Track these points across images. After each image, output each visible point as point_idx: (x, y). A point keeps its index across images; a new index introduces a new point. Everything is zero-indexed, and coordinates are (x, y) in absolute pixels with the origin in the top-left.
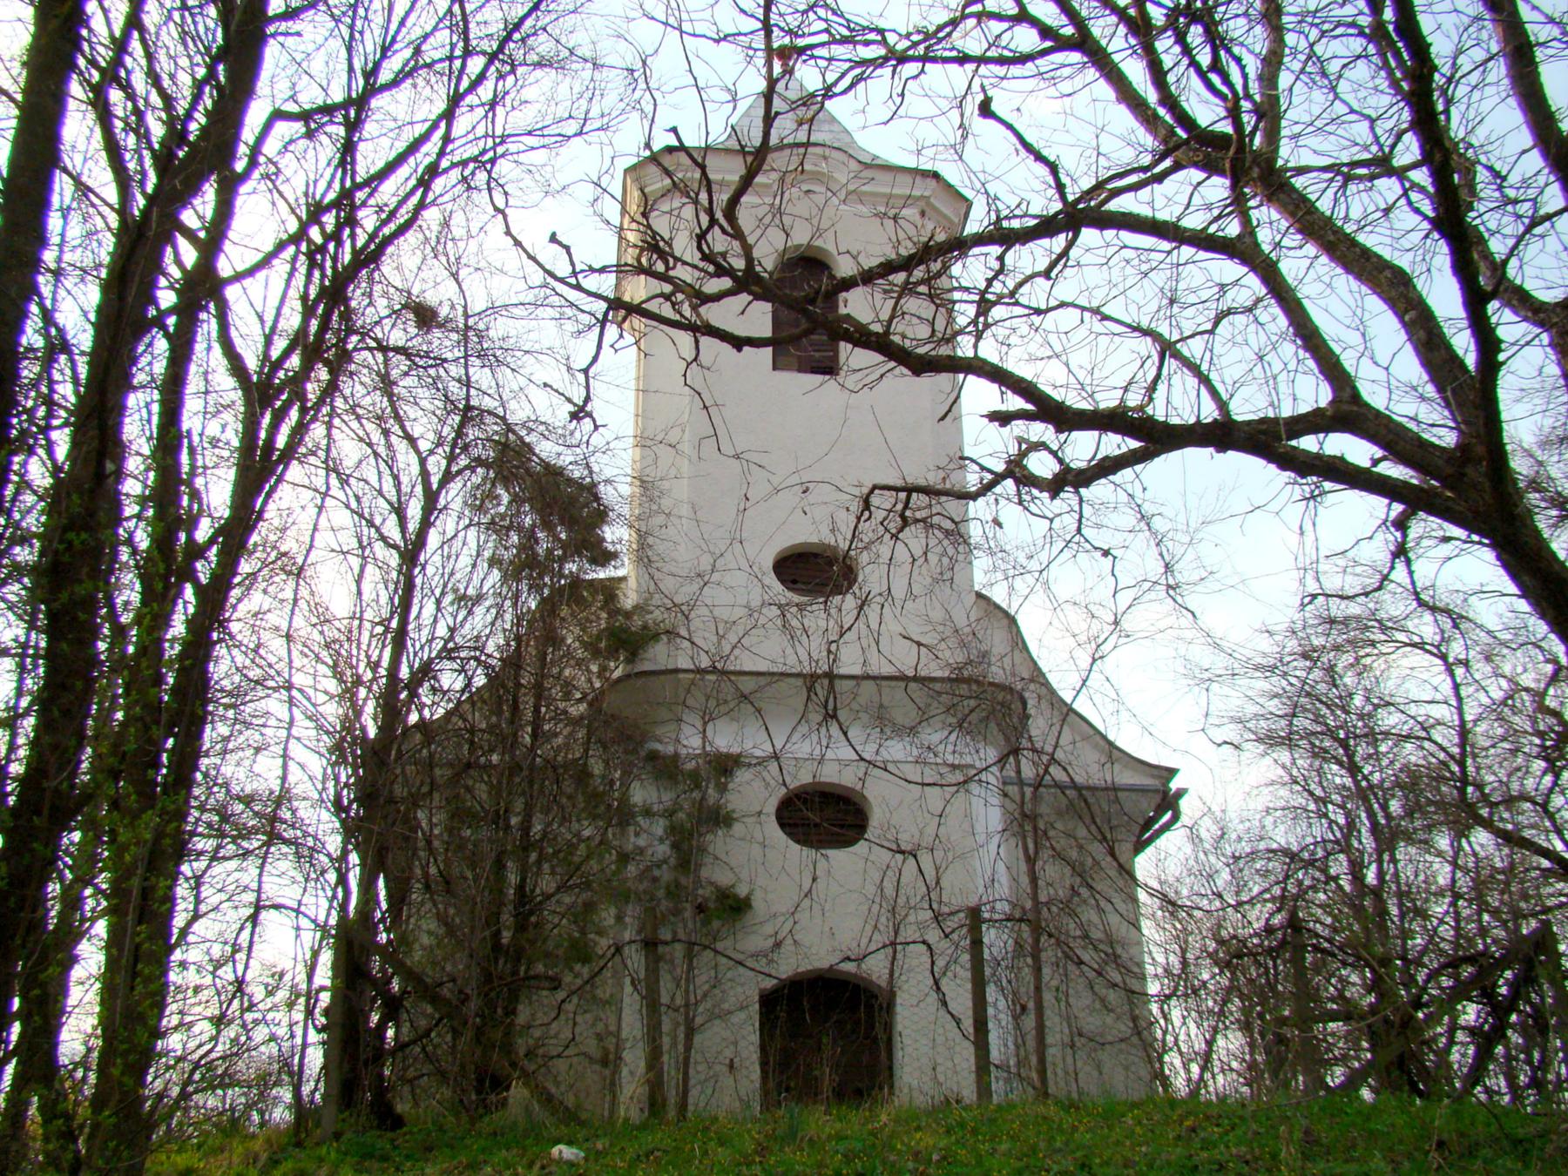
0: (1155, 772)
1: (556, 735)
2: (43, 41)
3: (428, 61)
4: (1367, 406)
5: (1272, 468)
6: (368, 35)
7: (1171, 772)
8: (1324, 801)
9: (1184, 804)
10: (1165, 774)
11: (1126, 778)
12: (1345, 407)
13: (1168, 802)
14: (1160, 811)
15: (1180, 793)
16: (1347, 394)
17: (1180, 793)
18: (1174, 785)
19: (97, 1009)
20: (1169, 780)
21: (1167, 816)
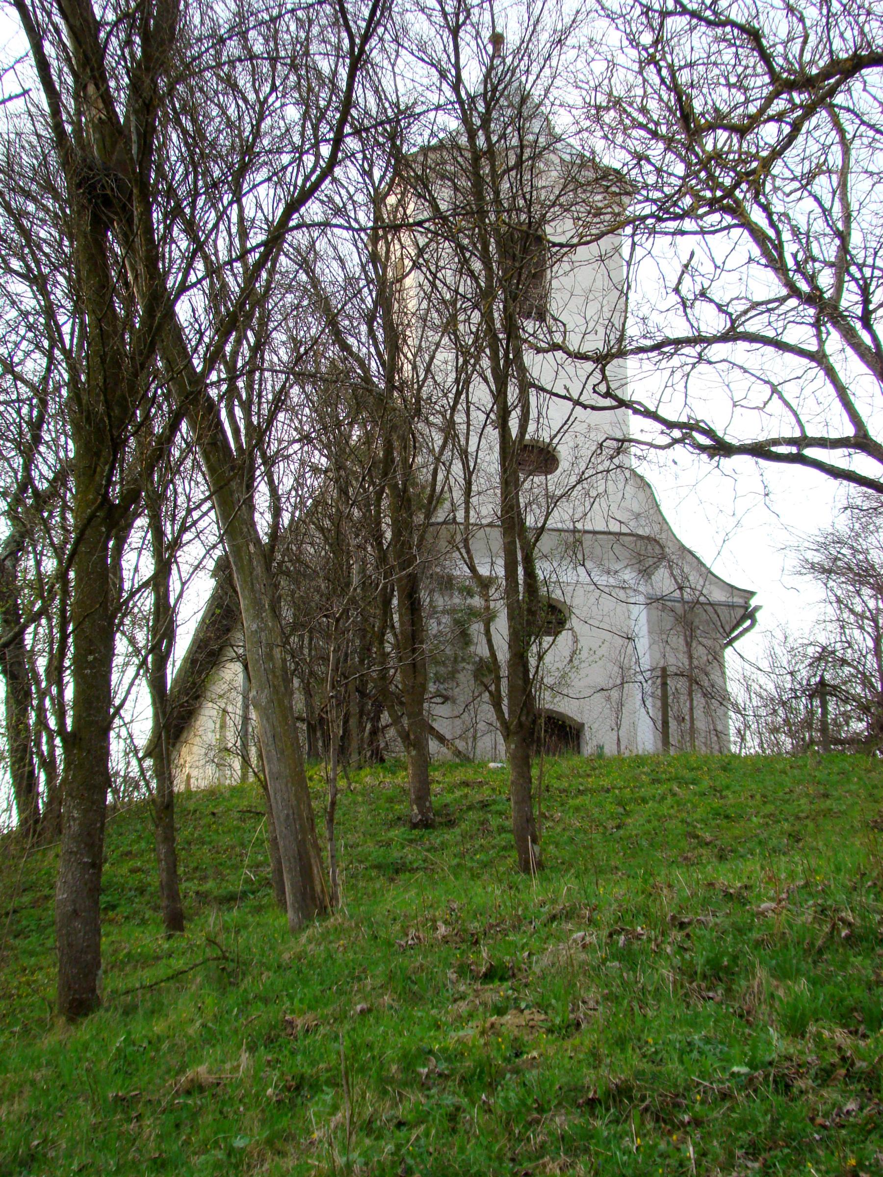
0: (742, 594)
1: (271, 361)
2: (534, 292)
3: (143, 552)
4: (871, 440)
5: (858, 472)
6: (177, 143)
7: (752, 594)
8: (862, 616)
9: (758, 615)
10: (746, 595)
11: (718, 596)
12: (860, 440)
13: (749, 615)
14: (743, 619)
15: (757, 608)
16: (861, 434)
17: (757, 608)
18: (753, 603)
19: (857, 75)
20: (749, 599)
21: (748, 623)
